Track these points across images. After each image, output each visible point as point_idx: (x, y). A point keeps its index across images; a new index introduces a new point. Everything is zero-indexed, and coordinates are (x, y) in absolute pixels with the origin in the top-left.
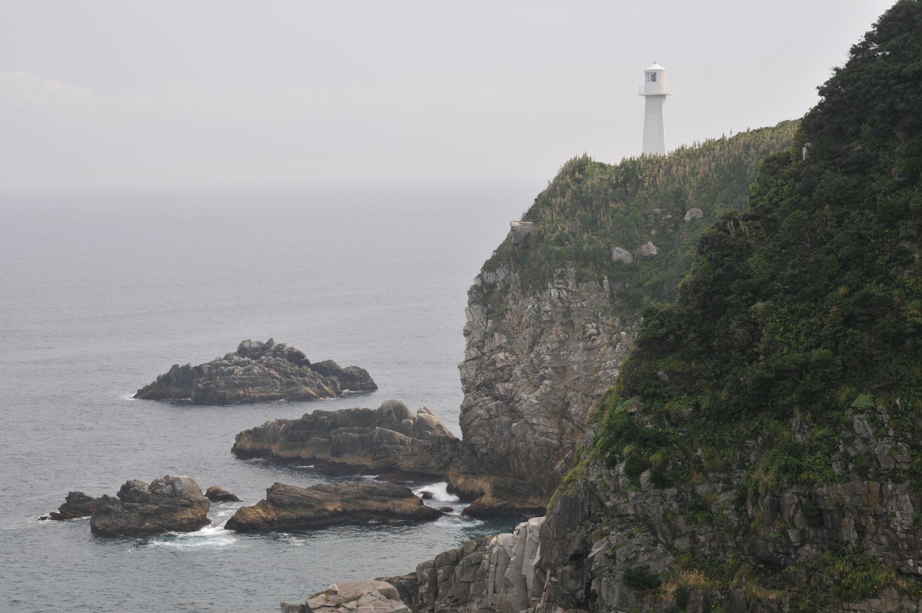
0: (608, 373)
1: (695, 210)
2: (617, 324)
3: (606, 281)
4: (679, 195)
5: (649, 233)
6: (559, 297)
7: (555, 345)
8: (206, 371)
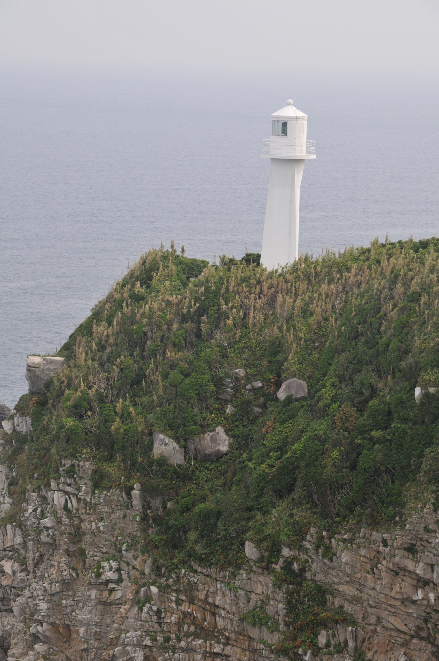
0: (128, 653)
1: (295, 381)
2: (147, 571)
4: (277, 348)
5: (222, 411)
6: (66, 508)
7: (56, 587)
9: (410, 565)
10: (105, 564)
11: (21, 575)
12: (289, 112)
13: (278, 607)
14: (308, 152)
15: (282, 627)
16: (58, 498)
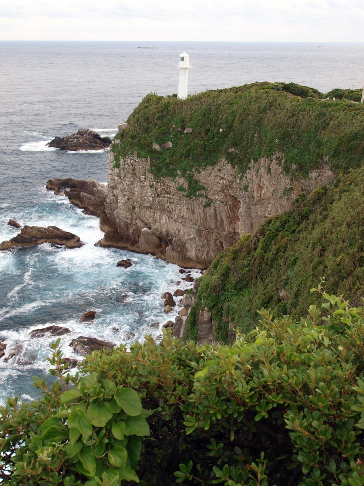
2: (152, 178)
3: (149, 158)
6: (131, 163)
8: (65, 140)
9: (219, 174)
10: (142, 177)
11: (120, 180)
12: (184, 55)
13: (186, 186)
14: (190, 65)
15: (187, 191)
16: (128, 161)
